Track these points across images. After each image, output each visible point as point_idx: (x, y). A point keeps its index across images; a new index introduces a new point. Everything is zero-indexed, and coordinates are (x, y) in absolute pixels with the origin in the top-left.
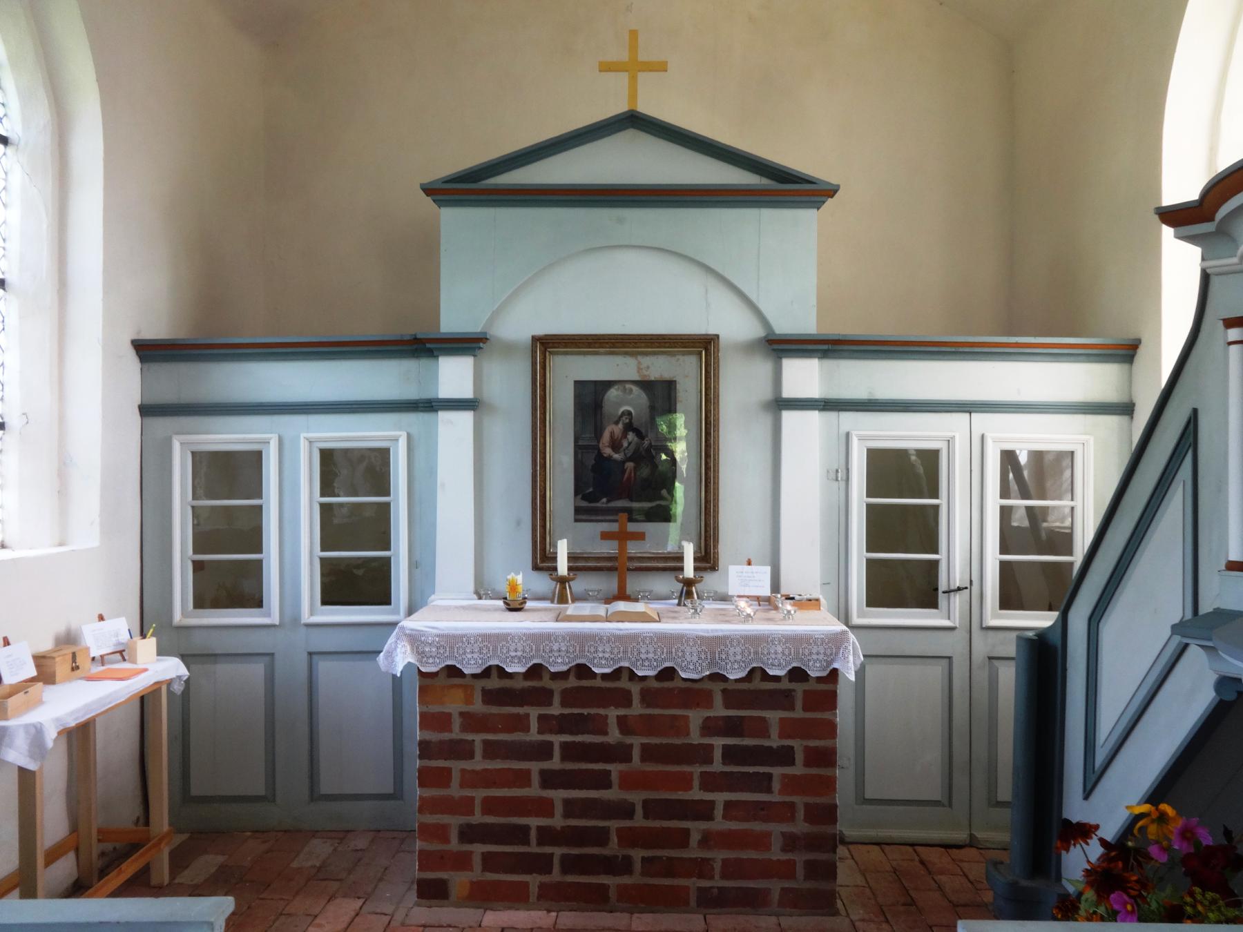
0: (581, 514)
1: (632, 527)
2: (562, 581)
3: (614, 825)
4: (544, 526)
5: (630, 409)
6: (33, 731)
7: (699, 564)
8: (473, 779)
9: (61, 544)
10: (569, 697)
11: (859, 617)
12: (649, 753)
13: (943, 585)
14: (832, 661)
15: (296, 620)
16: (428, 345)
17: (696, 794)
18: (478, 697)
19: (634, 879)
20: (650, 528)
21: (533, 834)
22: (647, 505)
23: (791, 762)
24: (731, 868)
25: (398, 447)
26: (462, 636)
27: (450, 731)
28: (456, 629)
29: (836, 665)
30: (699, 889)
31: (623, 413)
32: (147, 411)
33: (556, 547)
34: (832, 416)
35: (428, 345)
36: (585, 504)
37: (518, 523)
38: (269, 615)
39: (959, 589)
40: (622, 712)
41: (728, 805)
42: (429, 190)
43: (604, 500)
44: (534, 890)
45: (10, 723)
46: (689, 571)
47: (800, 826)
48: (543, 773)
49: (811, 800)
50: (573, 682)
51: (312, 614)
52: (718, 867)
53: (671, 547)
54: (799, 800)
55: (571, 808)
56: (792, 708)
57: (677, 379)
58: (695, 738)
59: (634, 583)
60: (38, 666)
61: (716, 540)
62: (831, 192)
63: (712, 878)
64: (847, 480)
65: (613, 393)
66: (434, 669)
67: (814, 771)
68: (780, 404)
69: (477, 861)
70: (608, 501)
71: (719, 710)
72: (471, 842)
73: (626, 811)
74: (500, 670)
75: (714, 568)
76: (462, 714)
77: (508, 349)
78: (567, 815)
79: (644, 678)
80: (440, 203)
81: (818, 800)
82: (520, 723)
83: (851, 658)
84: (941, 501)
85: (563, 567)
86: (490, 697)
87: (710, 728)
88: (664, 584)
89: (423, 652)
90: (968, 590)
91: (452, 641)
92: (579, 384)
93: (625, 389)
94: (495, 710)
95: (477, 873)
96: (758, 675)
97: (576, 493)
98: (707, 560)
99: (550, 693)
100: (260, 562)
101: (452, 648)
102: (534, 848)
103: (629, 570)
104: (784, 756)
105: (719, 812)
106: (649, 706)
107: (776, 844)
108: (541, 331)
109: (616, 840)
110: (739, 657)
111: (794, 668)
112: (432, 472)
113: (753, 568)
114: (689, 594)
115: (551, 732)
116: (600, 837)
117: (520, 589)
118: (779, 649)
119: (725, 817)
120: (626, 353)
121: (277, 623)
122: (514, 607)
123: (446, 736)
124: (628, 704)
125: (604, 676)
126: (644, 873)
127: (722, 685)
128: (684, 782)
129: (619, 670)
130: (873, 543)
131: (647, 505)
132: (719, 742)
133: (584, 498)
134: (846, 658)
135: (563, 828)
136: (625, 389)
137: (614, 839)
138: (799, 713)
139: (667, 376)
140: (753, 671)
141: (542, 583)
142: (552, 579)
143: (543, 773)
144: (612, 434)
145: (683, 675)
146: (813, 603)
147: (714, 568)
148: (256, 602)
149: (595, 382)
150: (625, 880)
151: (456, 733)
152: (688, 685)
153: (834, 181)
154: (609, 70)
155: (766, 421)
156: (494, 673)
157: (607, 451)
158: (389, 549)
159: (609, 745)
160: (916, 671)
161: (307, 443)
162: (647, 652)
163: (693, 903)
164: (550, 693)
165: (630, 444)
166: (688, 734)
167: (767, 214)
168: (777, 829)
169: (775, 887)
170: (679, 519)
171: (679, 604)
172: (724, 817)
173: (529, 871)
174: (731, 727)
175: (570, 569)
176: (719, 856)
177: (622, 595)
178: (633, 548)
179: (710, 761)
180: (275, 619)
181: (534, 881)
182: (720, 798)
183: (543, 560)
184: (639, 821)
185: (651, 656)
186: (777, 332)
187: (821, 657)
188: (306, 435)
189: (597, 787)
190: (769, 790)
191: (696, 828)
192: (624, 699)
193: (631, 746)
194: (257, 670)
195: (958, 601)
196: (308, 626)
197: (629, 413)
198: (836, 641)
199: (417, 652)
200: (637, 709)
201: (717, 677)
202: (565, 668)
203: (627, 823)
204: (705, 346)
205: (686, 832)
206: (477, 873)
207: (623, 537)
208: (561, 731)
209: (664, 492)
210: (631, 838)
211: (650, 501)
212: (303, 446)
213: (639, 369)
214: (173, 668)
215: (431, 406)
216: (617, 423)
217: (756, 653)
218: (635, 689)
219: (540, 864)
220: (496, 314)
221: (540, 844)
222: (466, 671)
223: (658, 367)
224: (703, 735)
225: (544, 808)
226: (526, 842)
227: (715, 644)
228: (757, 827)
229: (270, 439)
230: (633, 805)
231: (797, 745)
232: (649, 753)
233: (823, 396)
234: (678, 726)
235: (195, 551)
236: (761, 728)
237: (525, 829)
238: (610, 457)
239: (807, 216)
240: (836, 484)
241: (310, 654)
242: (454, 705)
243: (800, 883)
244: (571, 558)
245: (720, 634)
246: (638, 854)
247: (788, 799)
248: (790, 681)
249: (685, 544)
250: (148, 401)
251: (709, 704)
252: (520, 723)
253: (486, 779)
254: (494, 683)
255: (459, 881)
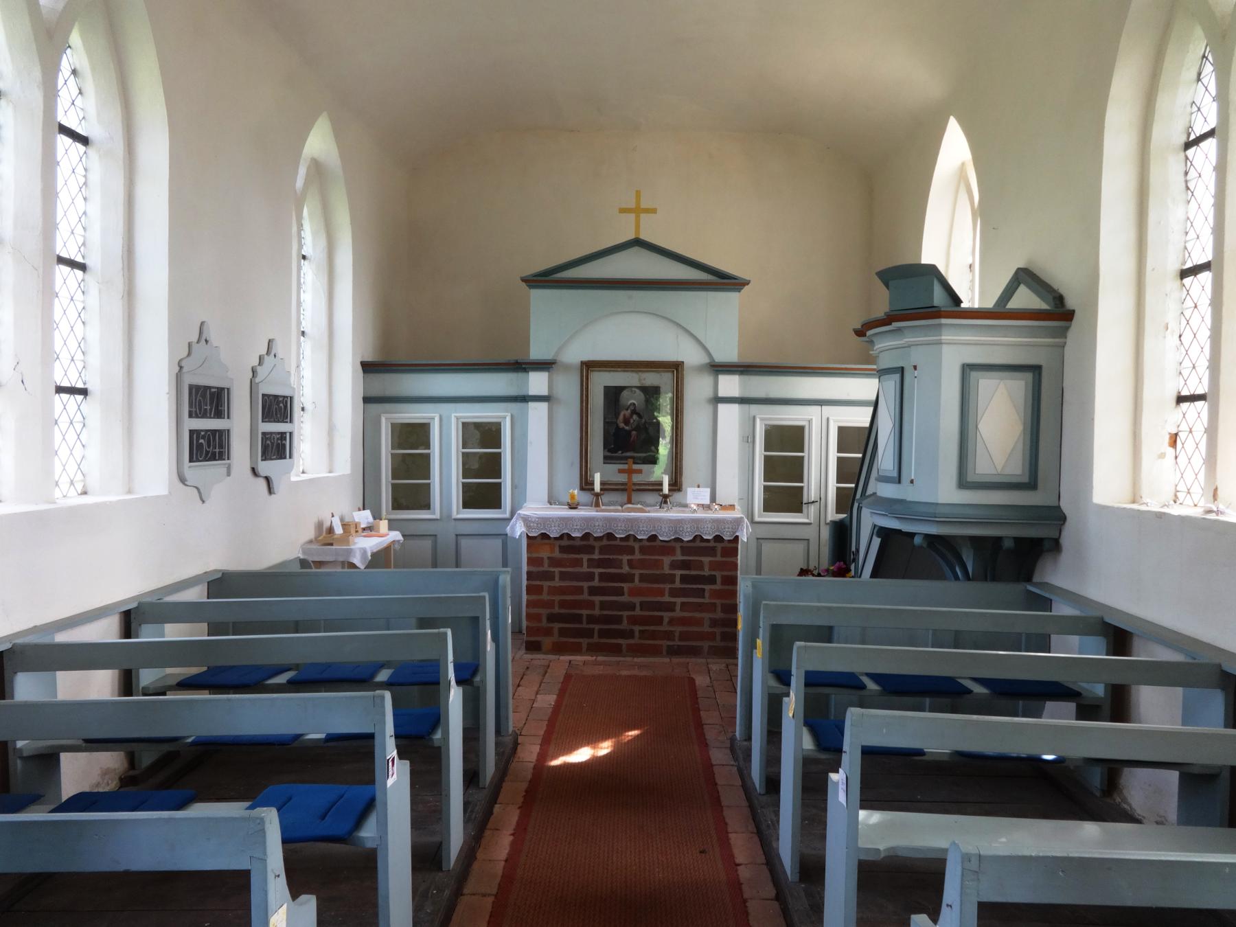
0: (607, 459)
1: (636, 467)
2: (597, 495)
3: (625, 614)
4: (586, 466)
5: (634, 402)
6: (362, 551)
7: (671, 488)
8: (553, 590)
9: (330, 472)
10: (603, 550)
11: (759, 517)
12: (643, 578)
13: (805, 500)
14: (735, 532)
15: (449, 516)
16: (523, 366)
17: (667, 598)
18: (557, 549)
19: (636, 641)
20: (645, 467)
21: (584, 619)
24: (684, 636)
25: (506, 422)
28: (547, 515)
29: (737, 534)
30: (668, 646)
31: (631, 404)
32: (367, 400)
33: (593, 477)
34: (746, 407)
35: (523, 366)
36: (609, 454)
37: (572, 464)
38: (434, 514)
39: (813, 502)
40: (629, 557)
41: (683, 604)
42: (525, 280)
43: (620, 452)
44: (585, 646)
45: (352, 547)
46: (666, 490)
47: (719, 615)
48: (589, 588)
49: (724, 602)
50: (605, 542)
51: (458, 513)
52: (677, 635)
53: (653, 478)
54: (718, 602)
57: (661, 386)
58: (667, 570)
59: (635, 496)
60: (344, 529)
61: (681, 475)
62: (746, 283)
64: (754, 442)
65: (625, 393)
66: (535, 535)
67: (727, 587)
68: (717, 400)
69: (556, 632)
70: (622, 453)
71: (679, 557)
72: (553, 622)
73: (632, 607)
74: (569, 535)
75: (679, 490)
76: (549, 558)
77: (567, 368)
79: (641, 540)
80: (531, 287)
81: (727, 602)
82: (578, 563)
83: (745, 530)
84: (805, 454)
85: (597, 488)
87: (674, 565)
88: (652, 498)
89: (530, 526)
90: (818, 503)
91: (545, 521)
93: (632, 391)
94: (565, 556)
95: (555, 638)
97: (605, 448)
98: (676, 485)
99: (593, 548)
100: (429, 485)
101: (544, 524)
102: (584, 625)
103: (634, 490)
104: (711, 580)
105: (678, 607)
106: (644, 554)
107: (707, 623)
108: (586, 358)
109: (626, 622)
110: (689, 530)
111: (716, 535)
112: (525, 435)
113: (701, 489)
114: (666, 502)
115: (594, 567)
117: (576, 497)
118: (709, 526)
119: (681, 610)
120: (632, 371)
122: (573, 507)
123: (541, 569)
125: (621, 539)
127: (681, 544)
128: (661, 593)
132: (678, 573)
133: (609, 451)
134: (742, 530)
135: (599, 615)
136: (632, 391)
137: (625, 622)
138: (719, 558)
141: (585, 497)
142: (592, 494)
144: (624, 415)
146: (732, 507)
147: (679, 490)
148: (426, 506)
149: (616, 387)
150: (631, 641)
152: (664, 544)
153: (748, 279)
154: (624, 212)
155: (709, 408)
156: (565, 537)
157: (622, 425)
158: (500, 478)
159: (623, 573)
160: (790, 546)
161: (456, 420)
162: (643, 527)
163: (664, 653)
164: (593, 548)
165: (634, 421)
166: (663, 568)
167: (711, 294)
168: (707, 616)
169: (706, 645)
170: (848, 752)
171: (660, 508)
172: (681, 610)
173: (582, 637)
174: (685, 565)
175: (601, 490)
177: (629, 502)
178: (636, 478)
179: (674, 582)
180: (437, 516)
181: (584, 642)
182: (679, 600)
183: (586, 485)
184: (638, 612)
185: (645, 529)
186: (716, 361)
187: (730, 530)
188: (455, 414)
189: (617, 595)
190: (703, 597)
191: (667, 615)
193: (634, 574)
194: (427, 543)
195: (813, 508)
196: (455, 520)
197: (634, 404)
198: (738, 522)
199: (527, 526)
200: (638, 556)
201: (678, 540)
202: (601, 535)
203: (632, 613)
204: (676, 368)
205: (662, 617)
206: (555, 638)
207: (630, 472)
208: (599, 567)
209: (653, 448)
210: (634, 620)
211: (646, 453)
212: (453, 421)
213: (640, 380)
214: (396, 536)
215: (525, 399)
217: (697, 528)
218: (637, 546)
219: (588, 633)
220: (560, 349)
221: (587, 623)
222: (551, 536)
223: (651, 379)
224: (670, 569)
226: (581, 623)
228: (697, 615)
229: (435, 416)
230: (635, 604)
231: (718, 574)
232: (643, 578)
233: (741, 396)
234: (658, 565)
235: (393, 479)
236: (700, 566)
237: (580, 616)
238: (623, 428)
239: (732, 297)
241: (457, 535)
242: (545, 554)
243: (718, 643)
244: (602, 483)
245: (680, 518)
246: (637, 628)
248: (715, 542)
249: (664, 476)
251: (674, 554)
253: (562, 591)
254: (565, 542)
255: (547, 642)
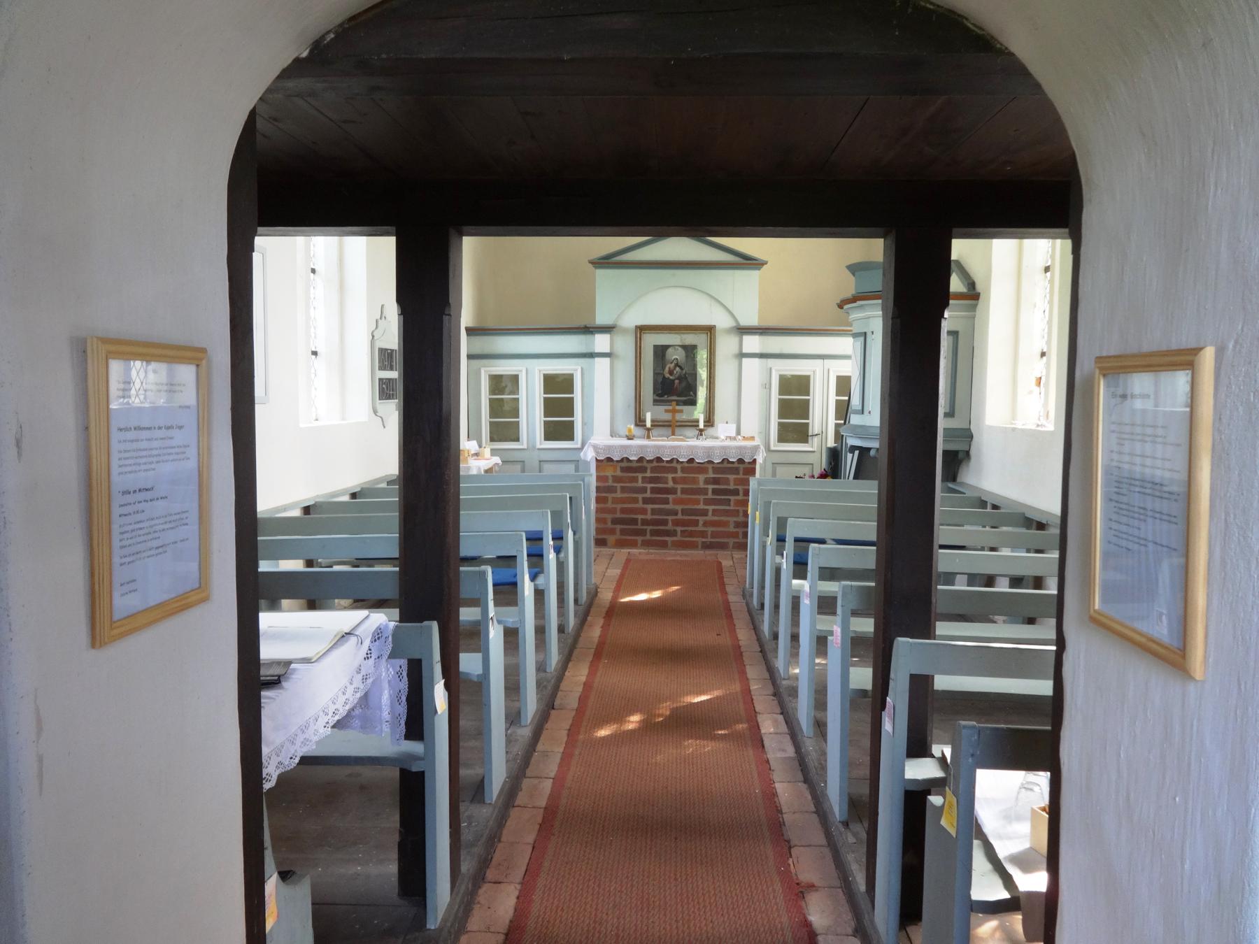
0: (656, 402)
2: (649, 430)
3: (670, 518)
5: (677, 357)
8: (615, 501)
10: (654, 470)
13: (810, 434)
15: (534, 447)
17: (702, 506)
18: (619, 469)
20: (685, 408)
22: (685, 398)
23: (738, 494)
24: (714, 535)
26: (613, 446)
27: (608, 482)
29: (755, 457)
33: (645, 416)
34: (764, 360)
36: (657, 398)
39: (816, 435)
40: (673, 475)
41: (714, 511)
43: (666, 396)
46: (701, 425)
48: (643, 498)
50: (655, 464)
51: (541, 444)
52: (709, 533)
55: (654, 511)
56: (738, 474)
58: (702, 485)
59: (677, 430)
63: (707, 538)
65: (670, 351)
68: (742, 355)
69: (618, 532)
71: (711, 475)
74: (627, 459)
75: (712, 426)
76: (612, 476)
77: (625, 331)
78: (652, 514)
80: (596, 268)
83: (761, 454)
85: (648, 424)
86: (624, 470)
92: (655, 347)
93: (675, 349)
95: (618, 536)
96: (726, 461)
97: (654, 393)
98: (710, 422)
103: (676, 426)
105: (710, 513)
107: (732, 526)
108: (640, 323)
114: (701, 435)
116: (665, 522)
121: (526, 448)
123: (607, 484)
124: (676, 472)
126: (681, 536)
127: (712, 465)
129: (673, 459)
130: (781, 415)
131: (685, 398)
132: (711, 487)
133: (657, 395)
137: (670, 523)
139: (694, 343)
140: (723, 460)
143: (643, 498)
144: (669, 368)
145: (697, 461)
147: (712, 426)
148: (517, 439)
150: (675, 539)
151: (610, 483)
152: (699, 465)
155: (736, 362)
157: (667, 375)
163: (700, 547)
166: (699, 484)
174: (715, 481)
176: (710, 529)
178: (678, 417)
180: (525, 446)
181: (640, 539)
182: (711, 508)
183: (640, 422)
184: (680, 516)
191: (701, 519)
192: (674, 470)
195: (816, 439)
196: (539, 449)
197: (677, 359)
200: (679, 474)
201: (710, 462)
202: (652, 458)
204: (709, 330)
207: (674, 412)
208: (650, 483)
210: (676, 523)
211: (685, 396)
212: (537, 372)
213: (681, 340)
215: (592, 355)
216: (672, 363)
217: (725, 453)
218: (679, 466)
220: (619, 316)
222: (615, 459)
223: (689, 339)
225: (644, 511)
227: (709, 450)
230: (677, 511)
232: (684, 491)
234: (695, 481)
236: (727, 481)
240: (765, 390)
241: (540, 461)
242: (609, 473)
244: (652, 421)
246: (679, 529)
247: (737, 508)
250: (470, 353)
252: (635, 480)
253: (622, 501)
254: (625, 464)
255: (611, 539)
